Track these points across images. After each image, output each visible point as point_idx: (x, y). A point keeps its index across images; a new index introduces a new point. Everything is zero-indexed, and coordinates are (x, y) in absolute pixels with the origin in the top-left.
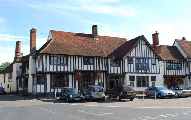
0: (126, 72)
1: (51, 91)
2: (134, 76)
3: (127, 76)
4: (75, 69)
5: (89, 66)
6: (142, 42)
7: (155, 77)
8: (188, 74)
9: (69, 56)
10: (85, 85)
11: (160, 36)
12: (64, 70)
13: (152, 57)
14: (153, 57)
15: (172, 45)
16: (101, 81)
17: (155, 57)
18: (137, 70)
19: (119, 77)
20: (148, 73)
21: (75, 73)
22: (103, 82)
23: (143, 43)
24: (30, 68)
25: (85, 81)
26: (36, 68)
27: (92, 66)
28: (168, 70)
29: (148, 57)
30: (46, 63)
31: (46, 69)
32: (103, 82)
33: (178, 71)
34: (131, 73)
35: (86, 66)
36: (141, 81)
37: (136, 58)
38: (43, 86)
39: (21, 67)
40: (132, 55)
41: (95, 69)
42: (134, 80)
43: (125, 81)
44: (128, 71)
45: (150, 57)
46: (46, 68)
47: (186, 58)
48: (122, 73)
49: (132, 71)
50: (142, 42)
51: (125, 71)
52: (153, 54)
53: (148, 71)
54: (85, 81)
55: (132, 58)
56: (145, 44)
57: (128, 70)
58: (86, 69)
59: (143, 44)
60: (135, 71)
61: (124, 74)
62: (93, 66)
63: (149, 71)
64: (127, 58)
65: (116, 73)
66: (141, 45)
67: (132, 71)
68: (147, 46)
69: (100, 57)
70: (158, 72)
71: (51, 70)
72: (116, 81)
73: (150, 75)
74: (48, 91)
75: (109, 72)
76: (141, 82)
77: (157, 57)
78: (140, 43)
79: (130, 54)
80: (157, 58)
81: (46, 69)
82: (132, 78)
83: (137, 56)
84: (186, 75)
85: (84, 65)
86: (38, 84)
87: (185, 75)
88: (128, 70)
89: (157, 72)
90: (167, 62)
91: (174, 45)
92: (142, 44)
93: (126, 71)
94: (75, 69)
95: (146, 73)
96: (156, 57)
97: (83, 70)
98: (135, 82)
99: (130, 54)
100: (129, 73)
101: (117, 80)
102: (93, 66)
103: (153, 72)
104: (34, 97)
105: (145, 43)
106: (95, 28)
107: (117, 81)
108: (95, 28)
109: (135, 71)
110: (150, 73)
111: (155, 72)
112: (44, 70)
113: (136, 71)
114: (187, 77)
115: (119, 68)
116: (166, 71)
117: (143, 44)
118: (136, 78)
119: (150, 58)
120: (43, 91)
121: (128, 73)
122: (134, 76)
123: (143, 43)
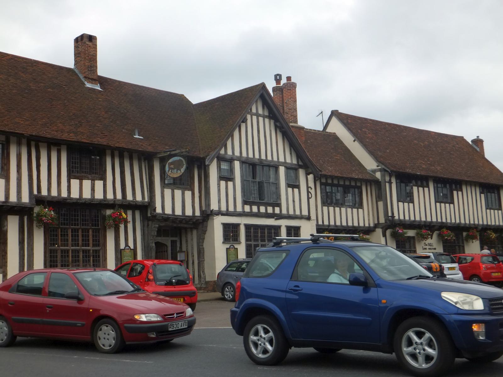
0: (212, 211)
2: (237, 226)
3: (218, 223)
4: (35, 192)
8: (382, 220)
9: (13, 139)
10: (259, 235)
15: (321, 128)
16: (127, 244)
17: (295, 162)
18: (245, 203)
19: (186, 229)
20: (280, 217)
22: (131, 245)
27: (99, 184)
28: (325, 208)
32: (131, 245)
34: (227, 214)
35: (75, 183)
37: (244, 162)
40: (230, 152)
41: (110, 196)
42: (236, 239)
43: (206, 245)
44: (220, 208)
47: (374, 171)
48: (198, 213)
51: (208, 205)
53: (277, 210)
54: (80, 242)
58: (75, 195)
62: (102, 182)
63: (281, 210)
65: (178, 212)
66: (255, 118)
68: (272, 122)
72: (169, 245)
73: (284, 223)
75: (159, 210)
77: (300, 163)
78: (254, 110)
79: (223, 149)
80: (301, 167)
83: (244, 154)
84: (376, 226)
87: (372, 225)
90: (323, 180)
91: (329, 130)
92: (258, 115)
93: (214, 206)
94: (35, 192)
96: (298, 162)
97: (65, 199)
99: (223, 149)
100: (223, 214)
101: (174, 239)
102: (102, 182)
104: (142, 270)
105: (266, 113)
106: (354, 141)
107: (173, 243)
108: (354, 141)
109: (239, 209)
110: (289, 217)
114: (379, 231)
115: (188, 194)
116: (398, 206)
121: (219, 213)
122: (279, 227)
123: (260, 111)
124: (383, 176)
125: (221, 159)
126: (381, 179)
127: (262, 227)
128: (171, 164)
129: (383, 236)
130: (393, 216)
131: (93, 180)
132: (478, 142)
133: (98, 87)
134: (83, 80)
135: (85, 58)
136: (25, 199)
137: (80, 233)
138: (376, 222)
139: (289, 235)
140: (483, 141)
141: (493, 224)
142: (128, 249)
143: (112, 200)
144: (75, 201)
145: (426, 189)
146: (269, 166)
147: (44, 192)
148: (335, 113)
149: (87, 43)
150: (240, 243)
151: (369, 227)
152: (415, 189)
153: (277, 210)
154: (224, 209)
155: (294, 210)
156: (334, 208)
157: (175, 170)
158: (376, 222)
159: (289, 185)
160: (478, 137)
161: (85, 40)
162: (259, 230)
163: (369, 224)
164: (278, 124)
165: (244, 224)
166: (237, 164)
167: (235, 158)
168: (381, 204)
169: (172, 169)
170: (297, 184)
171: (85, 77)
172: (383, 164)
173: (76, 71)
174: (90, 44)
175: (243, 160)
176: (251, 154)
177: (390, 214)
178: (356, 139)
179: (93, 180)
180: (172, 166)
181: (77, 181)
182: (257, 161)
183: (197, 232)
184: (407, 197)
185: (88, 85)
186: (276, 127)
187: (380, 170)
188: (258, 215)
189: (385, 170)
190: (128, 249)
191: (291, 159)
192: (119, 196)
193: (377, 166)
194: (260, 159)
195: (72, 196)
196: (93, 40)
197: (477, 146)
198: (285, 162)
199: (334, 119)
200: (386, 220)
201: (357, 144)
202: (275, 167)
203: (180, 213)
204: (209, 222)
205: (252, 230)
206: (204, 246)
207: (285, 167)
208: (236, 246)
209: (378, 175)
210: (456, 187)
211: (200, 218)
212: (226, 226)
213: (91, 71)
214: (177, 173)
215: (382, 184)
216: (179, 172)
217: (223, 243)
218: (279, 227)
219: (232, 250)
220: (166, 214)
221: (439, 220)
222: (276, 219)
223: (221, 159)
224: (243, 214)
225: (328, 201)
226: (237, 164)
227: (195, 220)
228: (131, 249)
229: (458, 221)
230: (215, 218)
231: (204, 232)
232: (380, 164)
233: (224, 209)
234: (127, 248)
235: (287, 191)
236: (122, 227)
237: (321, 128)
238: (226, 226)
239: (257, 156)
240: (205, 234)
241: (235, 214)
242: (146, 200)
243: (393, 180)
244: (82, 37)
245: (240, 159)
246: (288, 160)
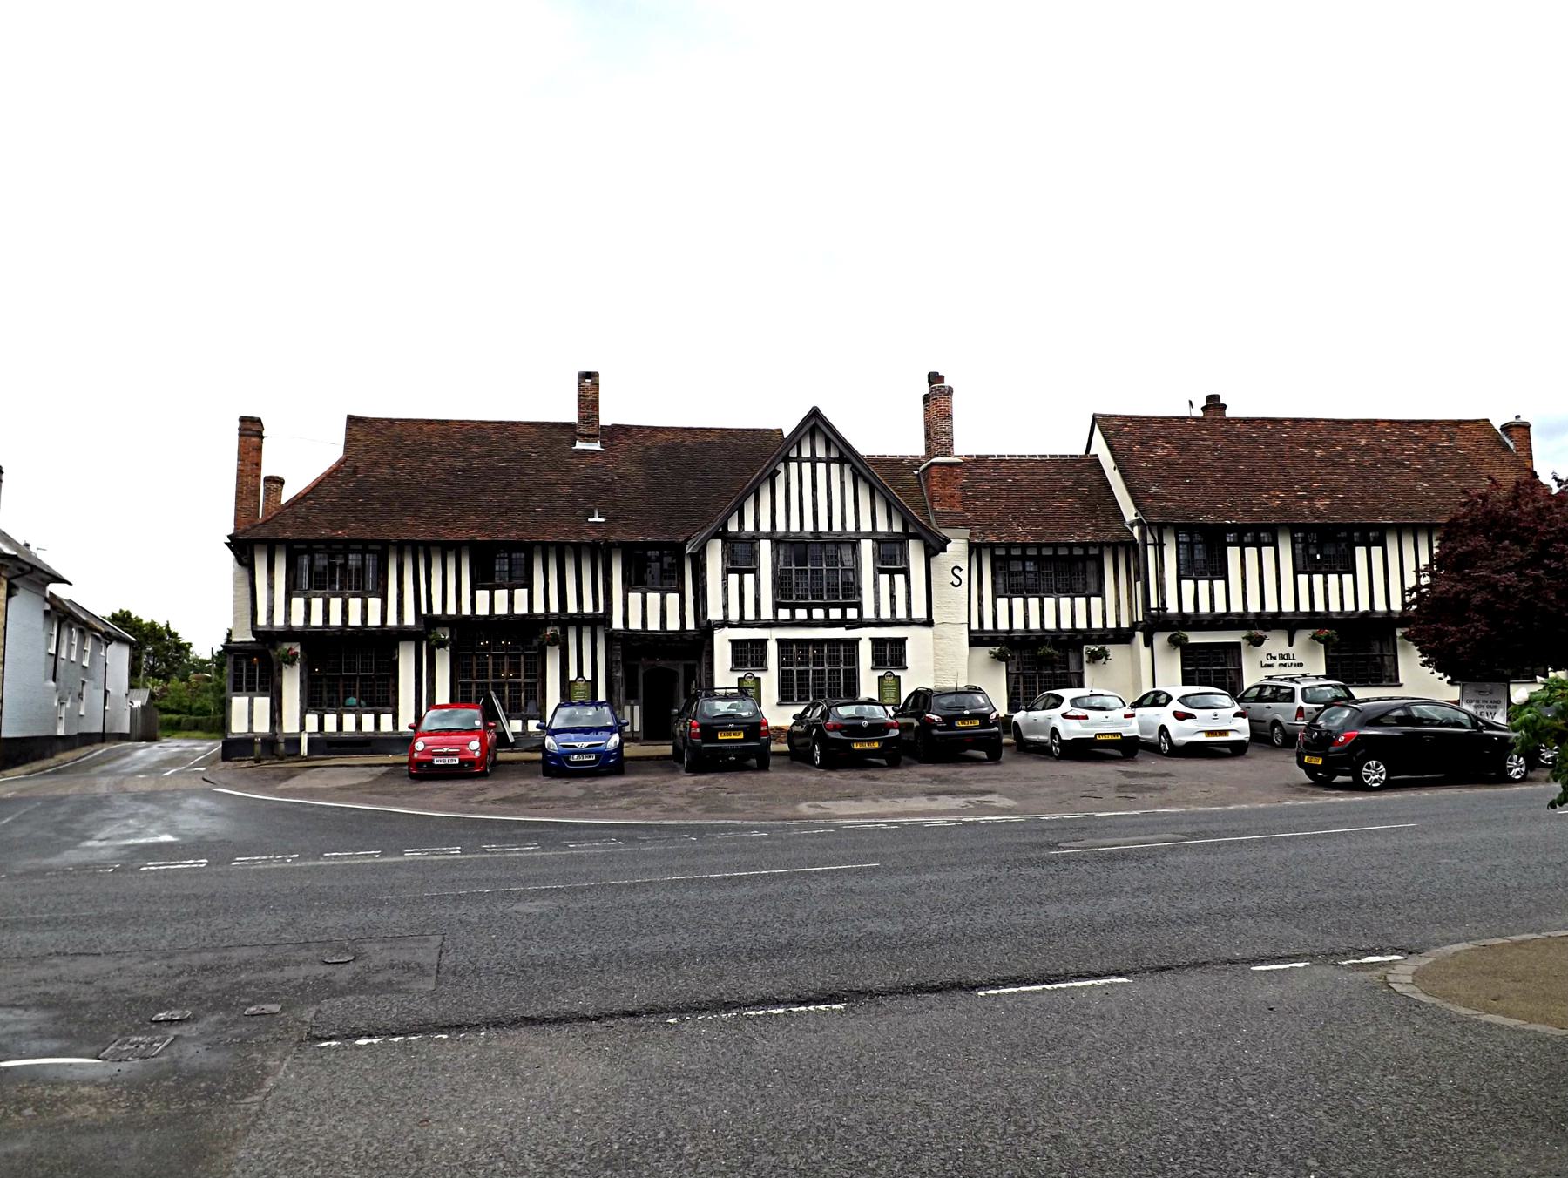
1: (302, 726)
3: (722, 643)
4: (424, 611)
5: (501, 595)
6: (813, 451)
7: (901, 642)
11: (825, 411)
13: (882, 527)
14: (890, 525)
15: (1082, 452)
17: (897, 528)
18: (777, 606)
20: (860, 623)
21: (426, 631)
22: (588, 675)
27: (521, 594)
29: (851, 527)
30: (271, 587)
32: (588, 675)
35: (482, 595)
37: (777, 541)
38: (263, 703)
40: (749, 527)
41: (539, 608)
42: (761, 664)
44: (726, 615)
45: (870, 529)
46: (271, 611)
48: (690, 625)
49: (750, 615)
50: (813, 451)
53: (852, 613)
54: (475, 674)
55: (755, 538)
56: (834, 461)
57: (725, 607)
59: (820, 460)
60: (767, 614)
61: (706, 630)
62: (1223, 582)
63: (860, 613)
64: (719, 543)
65: (654, 625)
67: (885, 614)
68: (847, 468)
69: (552, 544)
70: (919, 612)
71: (297, 620)
72: (681, 672)
73: (865, 635)
74: (290, 725)
78: (806, 453)
82: (748, 655)
84: (1134, 626)
86: (241, 690)
87: (1125, 624)
88: (725, 607)
89: (915, 615)
90: (1001, 552)
94: (424, 611)
95: (843, 622)
96: (905, 527)
98: (770, 681)
100: (732, 626)
103: (750, 615)
105: (834, 455)
110: (869, 624)
111: (901, 614)
113: (775, 613)
114: (1139, 636)
115: (673, 599)
117: (820, 460)
118: (772, 651)
119: (867, 536)
120: (262, 726)
121: (726, 623)
122: (856, 641)
123: (821, 453)
124: (1143, 533)
127: (818, 643)
129: (1146, 645)
132: (1519, 429)
133: (597, 446)
136: (410, 620)
137: (506, 661)
140: (128, 613)
143: (541, 614)
145: (1268, 552)
150: (766, 669)
153: (852, 613)
156: (1010, 598)
160: (1518, 417)
163: (1118, 623)
165: (777, 640)
166: (765, 547)
176: (792, 525)
181: (486, 593)
192: (554, 607)
195: (478, 613)
202: (854, 544)
203: (639, 627)
213: (588, 423)
217: (872, 669)
218: (856, 641)
224: (775, 624)
229: (1364, 606)
233: (734, 616)
237: (1082, 452)
238: (736, 644)
241: (758, 624)
242: (601, 610)
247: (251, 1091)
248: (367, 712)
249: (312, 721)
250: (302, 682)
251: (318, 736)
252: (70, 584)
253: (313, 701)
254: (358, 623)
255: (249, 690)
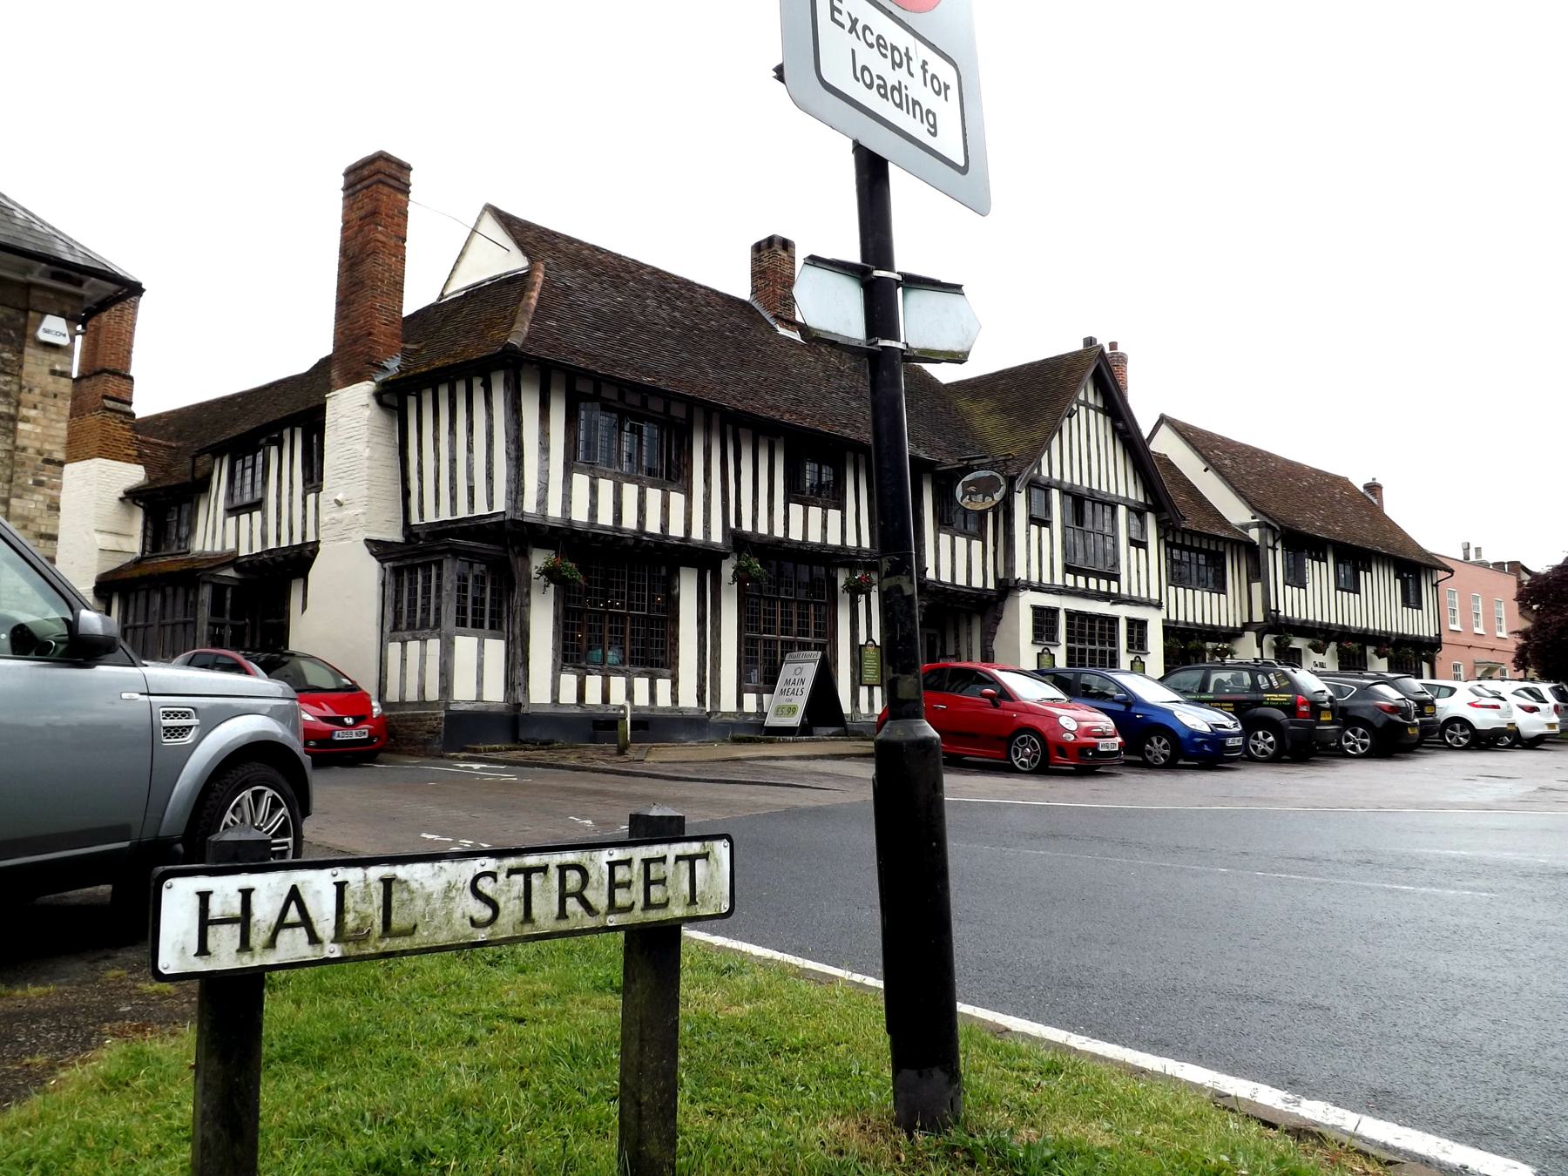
2: (1054, 612)
4: (733, 525)
8: (1258, 617)
12: (665, 525)
16: (869, 638)
17: (1141, 499)
18: (1068, 569)
20: (1117, 599)
23: (1091, 400)
24: (974, 659)
25: (795, 628)
26: (406, 494)
28: (232, 521)
30: (545, 449)
31: (542, 502)
33: (787, 529)
34: (1040, 588)
36: (1097, 647)
39: (132, 496)
40: (1045, 473)
42: (1052, 637)
46: (544, 488)
47: (1246, 527)
48: (991, 585)
52: (1135, 476)
54: (795, 628)
61: (1008, 588)
73: (1123, 612)
74: (539, 693)
76: (1085, 650)
77: (1149, 502)
78: (1082, 397)
80: (1150, 509)
81: (542, 502)
82: (1044, 621)
83: (1067, 479)
84: (1247, 627)
85: (788, 501)
87: (1239, 625)
92: (1088, 406)
93: (1020, 573)
94: (733, 525)
96: (1145, 499)
97: (779, 541)
100: (1034, 589)
106: (1206, 470)
108: (1206, 470)
109: (1058, 581)
112: (530, 505)
114: (1251, 637)
115: (977, 545)
121: (1028, 586)
123: (1091, 400)
124: (1262, 536)
125: (1033, 484)
126: (1260, 541)
128: (971, 483)
130: (1277, 611)
131: (825, 508)
133: (796, 336)
134: (772, 322)
135: (776, 281)
138: (1246, 620)
139: (1346, 666)
141: (1411, 633)
142: (871, 646)
144: (795, 546)
145: (1323, 564)
146: (1103, 503)
147: (747, 526)
148: (1163, 420)
149: (780, 253)
151: (1235, 628)
152: (1308, 562)
153: (1114, 589)
154: (1035, 579)
155: (1130, 590)
157: (980, 497)
158: (1246, 620)
159: (1133, 542)
160: (1374, 479)
161: (777, 246)
162: (1097, 622)
164: (1120, 425)
166: (1055, 494)
167: (1053, 484)
168: (1257, 587)
169: (971, 493)
170: (1144, 540)
171: (776, 317)
172: (1265, 514)
173: (756, 305)
174: (784, 255)
175: (1065, 487)
176: (1076, 477)
177: (1273, 607)
178: (1211, 467)
179: (825, 508)
180: (972, 489)
182: (1086, 493)
183: (982, 621)
184: (1296, 578)
185: (782, 331)
186: (1115, 430)
187: (1258, 525)
188: (1086, 594)
189: (1268, 526)
190: (871, 646)
191: (1135, 494)
193: (1253, 518)
194: (1090, 489)
196: (789, 249)
197: (1374, 495)
198: (1127, 498)
199: (1164, 428)
200: (1265, 618)
201: (1211, 476)
204: (1008, 604)
205: (1076, 622)
206: (994, 647)
207: (1127, 506)
208: (1053, 651)
209: (1254, 534)
210: (1363, 565)
211: (994, 594)
212: (1038, 611)
214: (984, 501)
215: (1262, 552)
216: (988, 499)
219: (1046, 656)
220: (956, 586)
221: (1340, 622)
222: (1113, 604)
223: (1033, 484)
224: (1063, 591)
225: (1177, 577)
226: (1055, 494)
227: (985, 597)
228: (876, 646)
230: (1021, 594)
231: (997, 620)
232: (1258, 514)
234: (870, 643)
235: (1128, 552)
236: (862, 598)
238: (1038, 611)
239: (1086, 484)
240: (997, 624)
243: (1279, 546)
244: (770, 241)
245: (1059, 486)
246: (1132, 496)
247: (167, 1157)
248: (640, 675)
249: (569, 682)
250: (556, 618)
251: (578, 710)
252: (853, 51)
253: (570, 655)
254: (657, 531)
255: (478, 624)
